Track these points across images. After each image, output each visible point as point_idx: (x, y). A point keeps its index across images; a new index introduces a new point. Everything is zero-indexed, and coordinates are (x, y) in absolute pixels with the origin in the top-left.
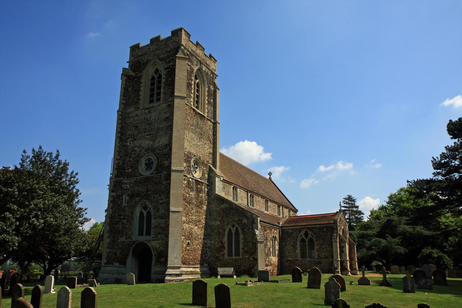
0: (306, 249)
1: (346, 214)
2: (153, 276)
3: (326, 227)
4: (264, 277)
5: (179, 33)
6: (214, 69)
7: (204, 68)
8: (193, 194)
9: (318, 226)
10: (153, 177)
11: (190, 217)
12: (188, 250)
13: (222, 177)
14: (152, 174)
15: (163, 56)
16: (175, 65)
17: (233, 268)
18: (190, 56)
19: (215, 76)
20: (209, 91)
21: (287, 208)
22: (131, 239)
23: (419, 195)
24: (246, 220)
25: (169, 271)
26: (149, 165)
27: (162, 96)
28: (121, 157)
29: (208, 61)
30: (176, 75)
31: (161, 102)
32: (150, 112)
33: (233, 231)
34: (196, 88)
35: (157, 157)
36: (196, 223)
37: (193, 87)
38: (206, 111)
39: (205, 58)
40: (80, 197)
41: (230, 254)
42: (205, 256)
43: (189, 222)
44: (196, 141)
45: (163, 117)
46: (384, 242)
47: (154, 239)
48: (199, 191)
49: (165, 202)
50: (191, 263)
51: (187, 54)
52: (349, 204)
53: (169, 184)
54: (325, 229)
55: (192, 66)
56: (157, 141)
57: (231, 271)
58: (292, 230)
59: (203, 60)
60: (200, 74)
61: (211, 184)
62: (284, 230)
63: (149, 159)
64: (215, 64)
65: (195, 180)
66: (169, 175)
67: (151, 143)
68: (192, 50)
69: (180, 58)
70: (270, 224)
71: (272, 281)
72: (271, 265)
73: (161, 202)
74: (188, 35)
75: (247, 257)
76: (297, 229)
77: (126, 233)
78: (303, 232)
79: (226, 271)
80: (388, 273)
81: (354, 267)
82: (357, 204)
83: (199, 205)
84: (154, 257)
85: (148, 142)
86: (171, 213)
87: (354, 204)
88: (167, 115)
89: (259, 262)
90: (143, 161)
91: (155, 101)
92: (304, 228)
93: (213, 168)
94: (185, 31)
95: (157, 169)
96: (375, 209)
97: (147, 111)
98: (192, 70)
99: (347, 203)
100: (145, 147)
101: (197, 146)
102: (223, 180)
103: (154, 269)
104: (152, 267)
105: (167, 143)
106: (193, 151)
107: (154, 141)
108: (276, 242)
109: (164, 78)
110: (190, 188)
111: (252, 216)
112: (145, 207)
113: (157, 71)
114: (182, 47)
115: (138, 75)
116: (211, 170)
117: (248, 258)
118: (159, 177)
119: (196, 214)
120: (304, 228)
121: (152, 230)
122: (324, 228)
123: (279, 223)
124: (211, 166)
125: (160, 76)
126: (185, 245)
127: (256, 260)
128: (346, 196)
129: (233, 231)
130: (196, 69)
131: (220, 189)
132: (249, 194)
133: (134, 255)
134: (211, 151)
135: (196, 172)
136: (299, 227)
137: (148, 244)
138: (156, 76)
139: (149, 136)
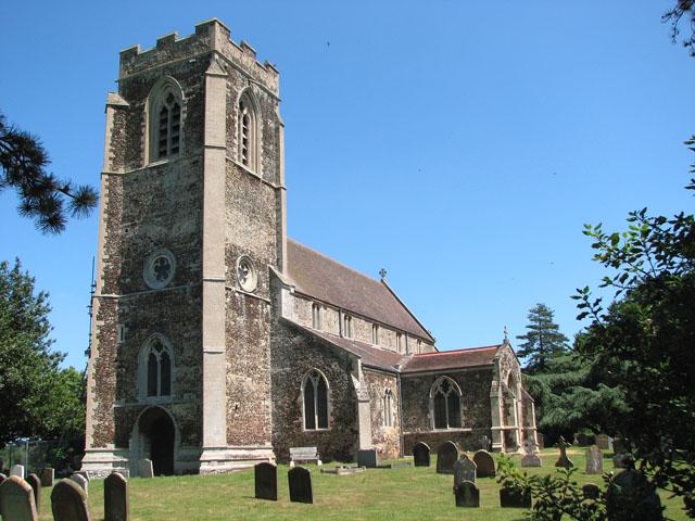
0: (445, 412)
1: (535, 340)
2: (177, 465)
3: (480, 372)
4: (367, 460)
5: (210, 29)
7: (256, 89)
8: (241, 320)
10: (170, 292)
14: (168, 286)
16: (203, 88)
17: (315, 448)
18: (231, 69)
20: (264, 131)
21: (413, 336)
22: (137, 401)
23: (630, 313)
24: (336, 363)
25: (206, 455)
26: (162, 269)
27: (182, 144)
29: (263, 75)
30: (207, 108)
32: (160, 173)
33: (315, 384)
34: (242, 126)
35: (176, 256)
36: (250, 370)
37: (236, 125)
38: (262, 167)
39: (257, 69)
40: (51, 335)
41: (310, 424)
44: (244, 225)
45: (185, 184)
46: (597, 395)
47: (177, 401)
48: (252, 314)
49: (194, 337)
52: (540, 321)
53: (201, 304)
54: (478, 376)
56: (175, 227)
57: (312, 453)
58: (420, 378)
59: (254, 73)
61: (275, 303)
63: (162, 260)
65: (246, 295)
66: (200, 289)
67: (164, 230)
68: (233, 58)
69: (211, 75)
70: (378, 371)
71: (379, 467)
72: (383, 441)
73: (186, 335)
74: (227, 32)
75: (340, 428)
76: (429, 376)
77: (126, 392)
78: (439, 381)
80: (568, 446)
83: (254, 338)
84: (177, 432)
85: (159, 228)
86: (205, 355)
88: (193, 180)
89: (361, 436)
90: (151, 263)
91: (168, 153)
93: (277, 272)
95: (176, 278)
97: (155, 172)
98: (234, 94)
99: (535, 320)
101: (247, 233)
103: (179, 452)
104: (176, 449)
105: (193, 231)
106: (239, 243)
108: (392, 401)
109: (184, 112)
111: (347, 357)
112: (159, 346)
113: (171, 98)
114: (217, 56)
115: (137, 105)
116: (273, 276)
117: (342, 430)
118: (181, 291)
122: (475, 373)
123: (397, 367)
124: (272, 267)
125: (177, 107)
127: (357, 433)
129: (315, 384)
131: (290, 309)
132: (343, 315)
134: (273, 240)
135: (245, 280)
136: (432, 373)
137: (168, 411)
138: (169, 108)
139: (160, 219)
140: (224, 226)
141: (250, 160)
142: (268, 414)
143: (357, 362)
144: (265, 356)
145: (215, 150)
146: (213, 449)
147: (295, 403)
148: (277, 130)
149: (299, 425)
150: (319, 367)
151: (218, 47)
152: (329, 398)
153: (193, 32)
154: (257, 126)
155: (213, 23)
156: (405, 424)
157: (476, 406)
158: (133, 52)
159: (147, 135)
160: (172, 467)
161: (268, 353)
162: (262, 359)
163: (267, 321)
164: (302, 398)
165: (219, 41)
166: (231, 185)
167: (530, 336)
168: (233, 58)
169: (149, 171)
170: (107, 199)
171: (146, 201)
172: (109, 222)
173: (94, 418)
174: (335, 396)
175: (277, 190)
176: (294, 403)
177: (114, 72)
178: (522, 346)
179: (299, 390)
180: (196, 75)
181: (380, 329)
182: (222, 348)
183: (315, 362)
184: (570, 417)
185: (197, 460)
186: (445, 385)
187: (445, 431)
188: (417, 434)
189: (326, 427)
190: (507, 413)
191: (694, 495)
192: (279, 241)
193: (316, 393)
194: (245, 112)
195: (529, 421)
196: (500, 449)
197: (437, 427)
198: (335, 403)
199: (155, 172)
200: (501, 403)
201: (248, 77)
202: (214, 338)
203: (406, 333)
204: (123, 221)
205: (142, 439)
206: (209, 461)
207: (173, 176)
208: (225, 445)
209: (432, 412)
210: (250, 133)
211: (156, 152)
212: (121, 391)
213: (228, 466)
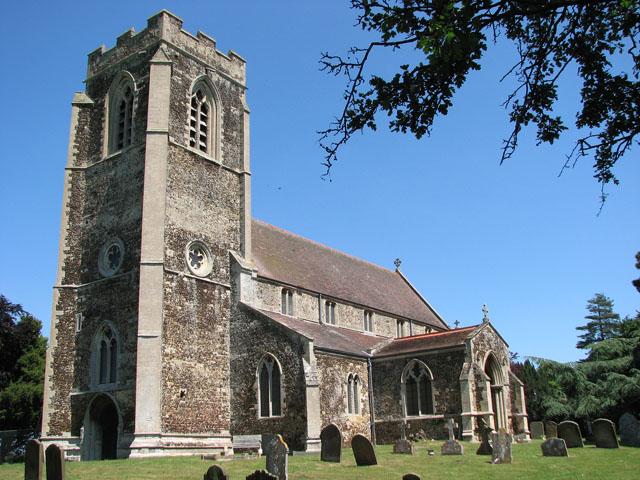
3: (452, 354)
6: (239, 76)
7: (215, 78)
8: (191, 305)
9: (436, 352)
11: (186, 347)
12: (182, 406)
13: (255, 271)
14: (116, 274)
15: (135, 64)
17: (260, 436)
19: (240, 89)
22: (88, 389)
24: (289, 347)
25: (137, 442)
26: (114, 258)
28: (72, 248)
31: (132, 145)
32: (115, 164)
33: (270, 370)
38: (222, 153)
39: (217, 58)
41: (265, 412)
42: (223, 417)
43: (184, 355)
48: (205, 300)
50: (190, 429)
51: (176, 56)
52: (600, 311)
54: (449, 358)
55: (187, 76)
58: (392, 362)
59: (214, 62)
60: (208, 89)
61: (235, 289)
62: (378, 363)
63: (115, 248)
64: (242, 68)
65: (197, 280)
68: (186, 48)
69: (156, 63)
74: (179, 23)
75: (292, 415)
76: (400, 360)
78: (410, 365)
79: (248, 441)
81: (520, 428)
82: (615, 311)
83: (209, 322)
84: (120, 420)
85: (113, 217)
86: (139, 339)
87: (610, 311)
90: (105, 251)
92: (411, 358)
93: (237, 257)
94: (170, 16)
95: (124, 265)
96: (630, 318)
97: (111, 163)
99: (594, 310)
100: (108, 228)
101: (200, 218)
102: (258, 276)
106: (190, 228)
107: (120, 215)
110: (185, 296)
111: (299, 339)
114: (164, 46)
116: (233, 260)
119: (200, 341)
120: (411, 358)
121: (118, 372)
122: (446, 355)
123: (369, 351)
124: (233, 253)
126: (174, 397)
128: (593, 297)
130: (194, 80)
131: (249, 293)
132: (324, 301)
133: (93, 418)
134: (236, 225)
135: (199, 265)
136: (404, 356)
137: (113, 398)
140: (165, 208)
141: (209, 147)
142: (225, 401)
143: (308, 345)
144: (223, 342)
145: (157, 135)
146: (146, 436)
147: (251, 391)
148: (242, 116)
149: (255, 411)
150: (273, 352)
151: (166, 36)
152: (282, 384)
153: (146, 26)
154: (216, 114)
155: (161, 15)
156: (376, 408)
157: (447, 390)
158: (98, 53)
159: (107, 129)
160: (115, 453)
161: (227, 339)
162: (218, 346)
163: (225, 306)
164: (258, 384)
165: (167, 30)
166: (181, 170)
167: (590, 326)
168: (186, 48)
169: (106, 164)
170: (70, 194)
171: (103, 192)
172: (71, 215)
173: (51, 406)
174: (288, 381)
175: (241, 176)
176: (250, 390)
177: (82, 72)
178: (583, 337)
179: (254, 376)
180: (143, 68)
181: (374, 316)
182: (159, 332)
183: (269, 346)
184: (603, 406)
185: (128, 449)
186: (417, 369)
187: (416, 418)
188: (390, 422)
189: (279, 414)
190: (479, 398)
191: (1, 414)
192: (243, 227)
193: (270, 377)
194: (204, 100)
195: (517, 407)
196: (470, 437)
197: (409, 414)
198: (288, 388)
199: (111, 163)
200: (471, 386)
201: (206, 66)
202: (150, 319)
203: (409, 320)
204: (85, 213)
205: (93, 427)
206: (140, 448)
207: (125, 166)
208: (159, 431)
209: (404, 397)
210: (210, 121)
211: (115, 144)
212: (80, 379)
213: (159, 453)
